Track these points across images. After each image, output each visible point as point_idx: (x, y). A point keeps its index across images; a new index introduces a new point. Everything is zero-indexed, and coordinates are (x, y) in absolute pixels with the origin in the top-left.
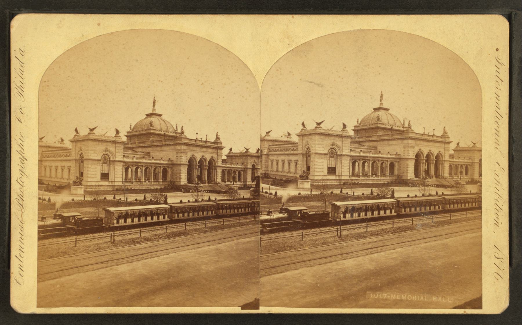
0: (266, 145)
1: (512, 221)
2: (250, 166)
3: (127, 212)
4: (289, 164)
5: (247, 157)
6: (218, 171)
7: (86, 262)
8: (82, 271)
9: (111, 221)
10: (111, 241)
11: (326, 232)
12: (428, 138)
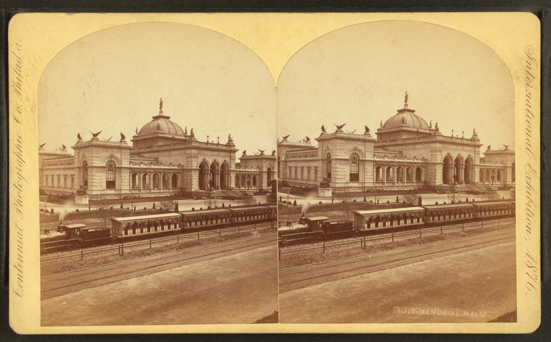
0: (284, 151)
1: (544, 232)
2: (265, 169)
3: (135, 222)
4: (309, 171)
5: (262, 160)
6: (231, 175)
7: (93, 277)
8: (89, 286)
9: (118, 232)
10: (119, 253)
11: (349, 243)
12: (458, 141)
